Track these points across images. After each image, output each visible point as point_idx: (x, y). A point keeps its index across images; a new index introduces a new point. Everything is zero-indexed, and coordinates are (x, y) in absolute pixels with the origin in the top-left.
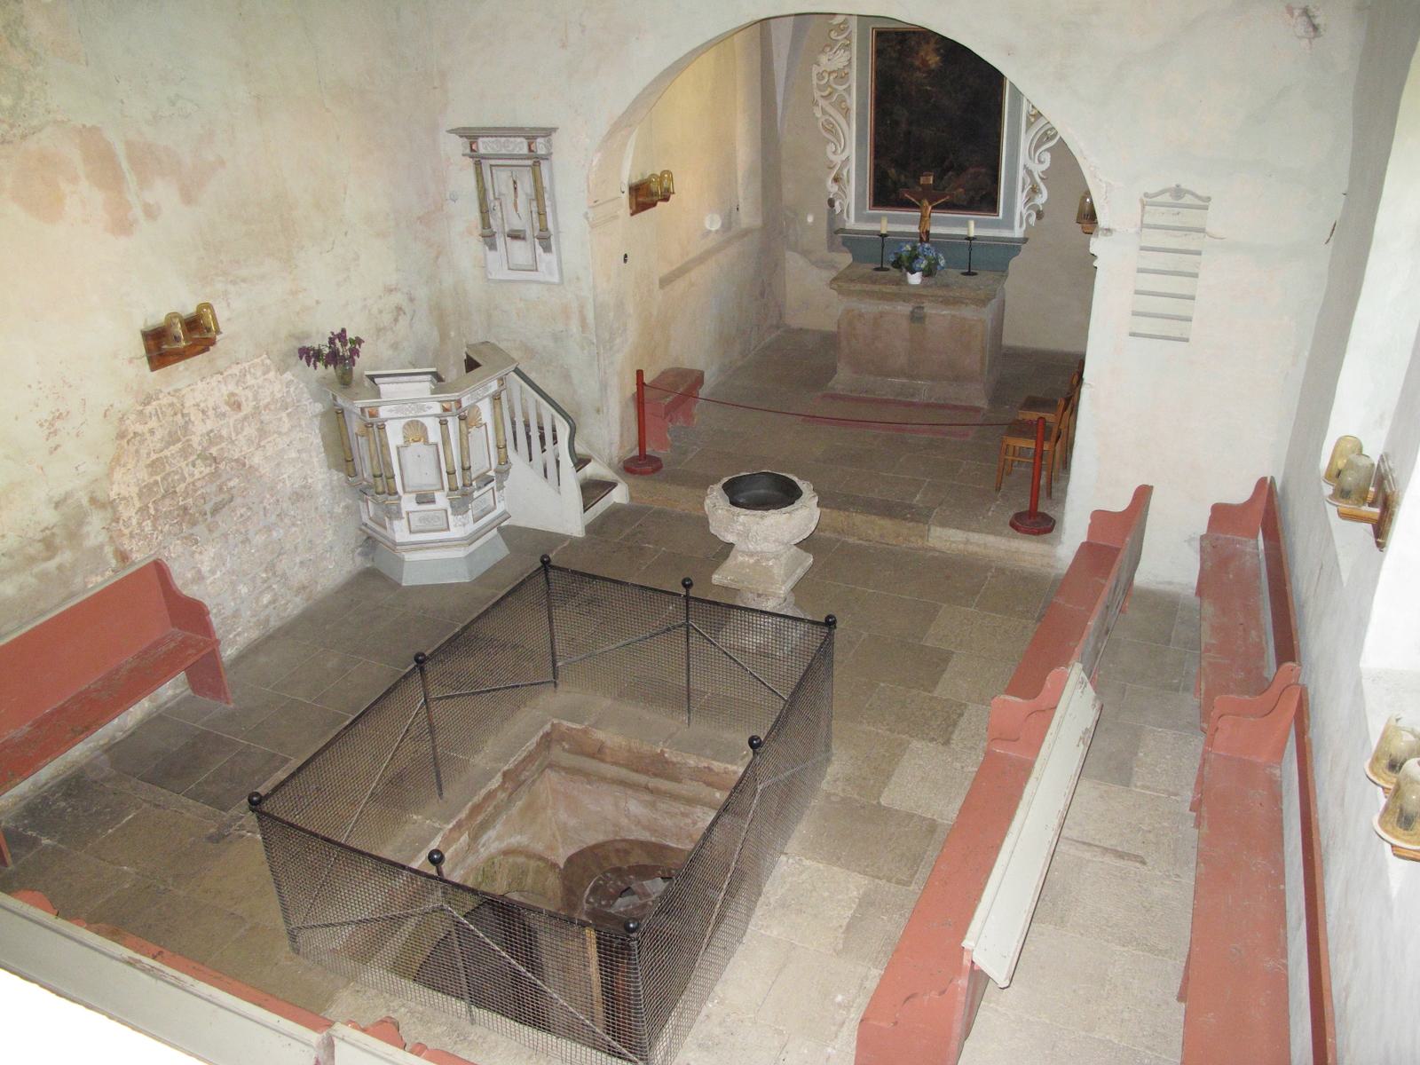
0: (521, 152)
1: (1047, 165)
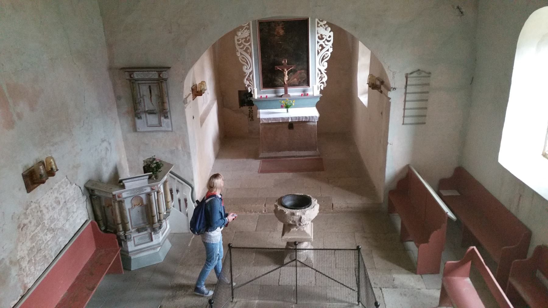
1: (326, 67)
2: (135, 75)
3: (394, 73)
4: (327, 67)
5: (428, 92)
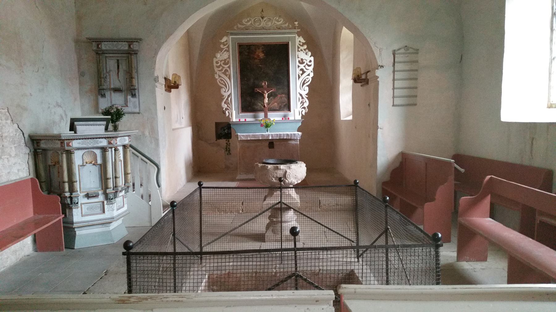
2: (103, 45)
3: (381, 50)
4: (308, 92)
5: (417, 70)
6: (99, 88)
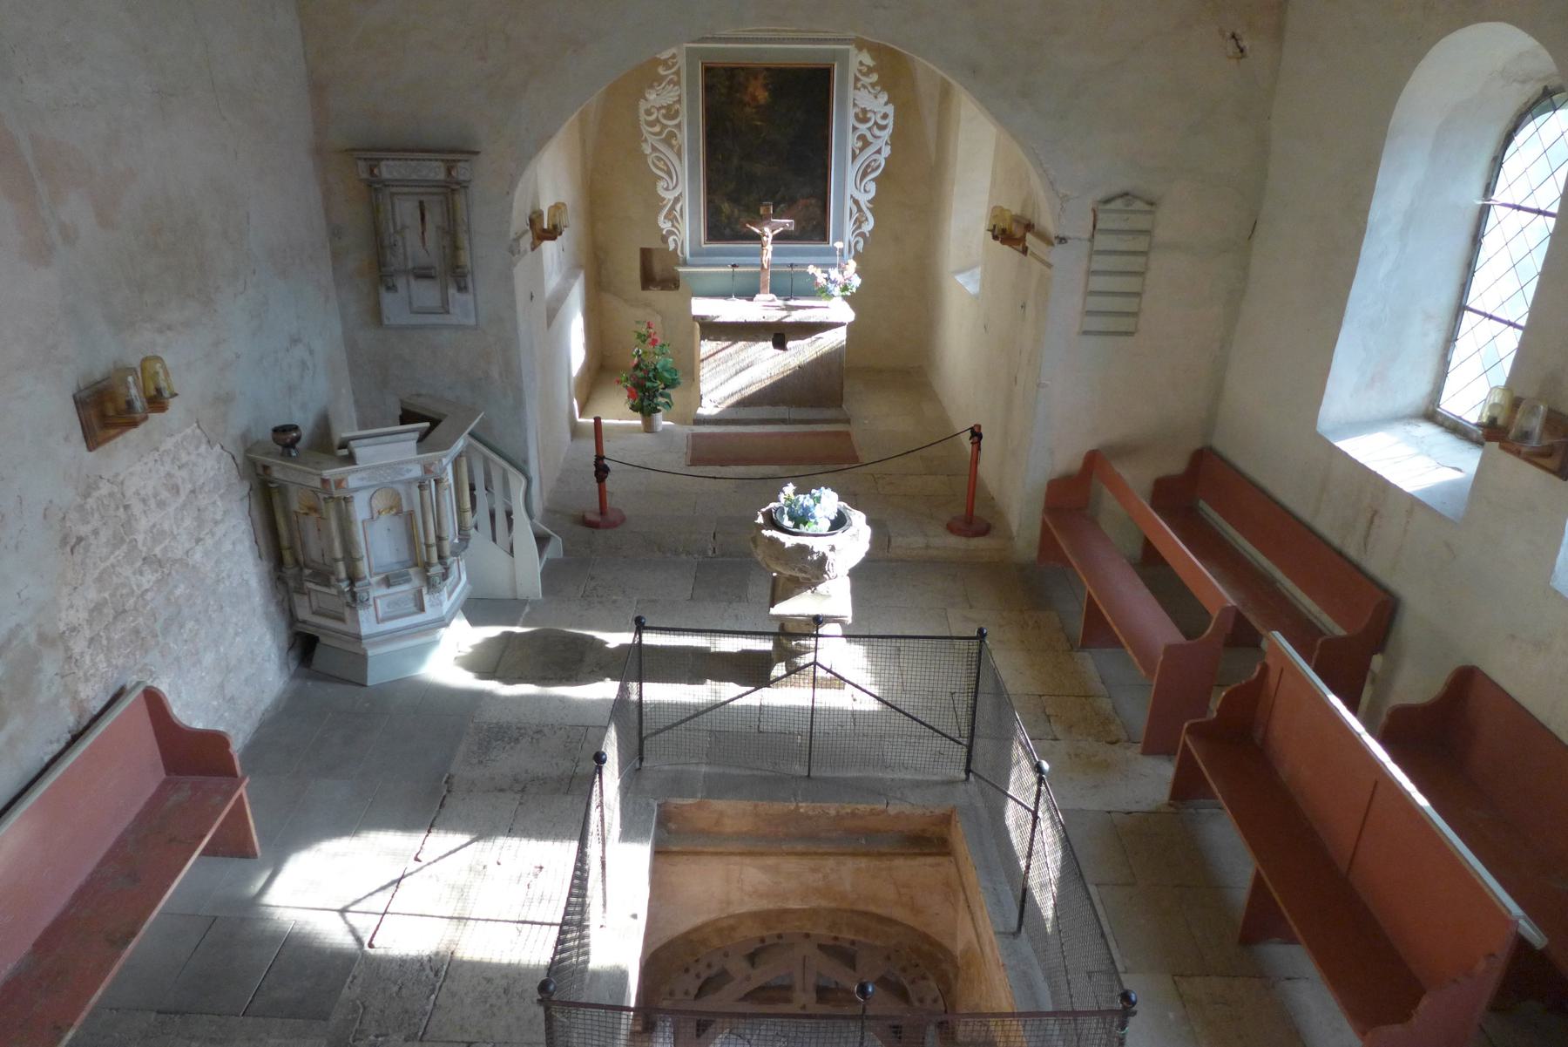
0: (438, 178)
1: (872, 194)
6: (380, 271)
